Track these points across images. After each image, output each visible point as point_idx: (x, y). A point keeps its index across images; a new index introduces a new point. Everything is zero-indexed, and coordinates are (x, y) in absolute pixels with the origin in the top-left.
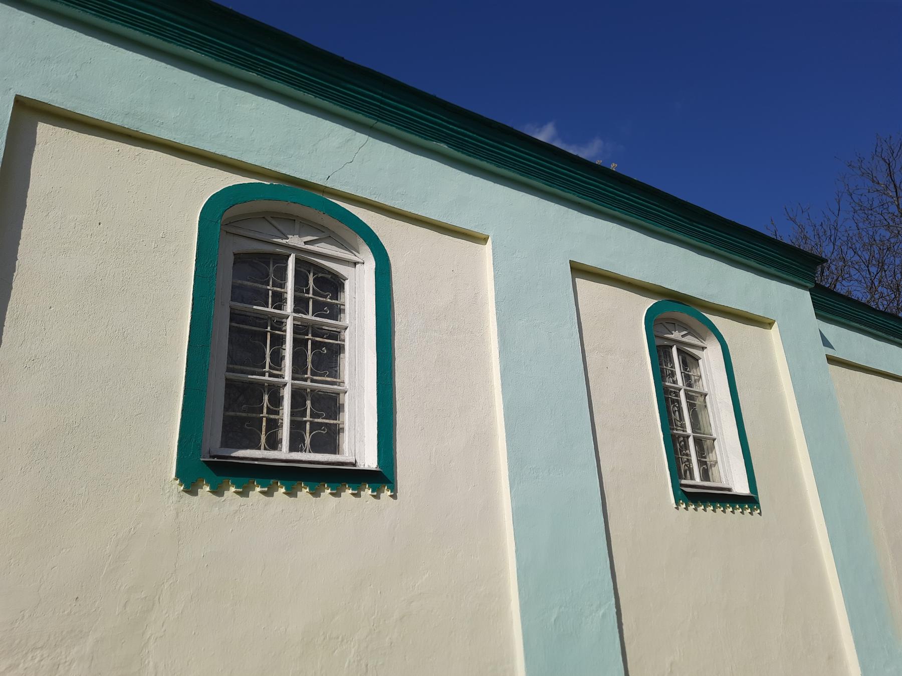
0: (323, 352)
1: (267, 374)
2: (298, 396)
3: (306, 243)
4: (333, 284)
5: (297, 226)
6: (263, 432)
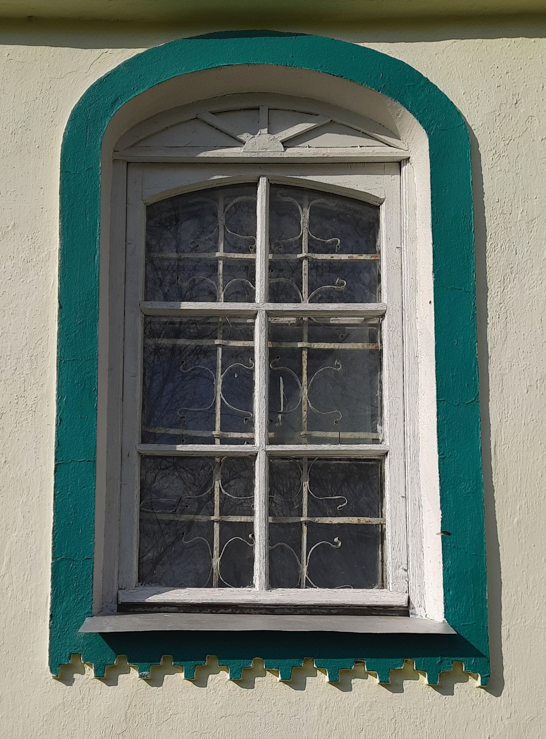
0: (336, 372)
1: (218, 441)
2: (282, 472)
3: (286, 144)
4: (359, 220)
5: (263, 115)
6: (305, 377)
